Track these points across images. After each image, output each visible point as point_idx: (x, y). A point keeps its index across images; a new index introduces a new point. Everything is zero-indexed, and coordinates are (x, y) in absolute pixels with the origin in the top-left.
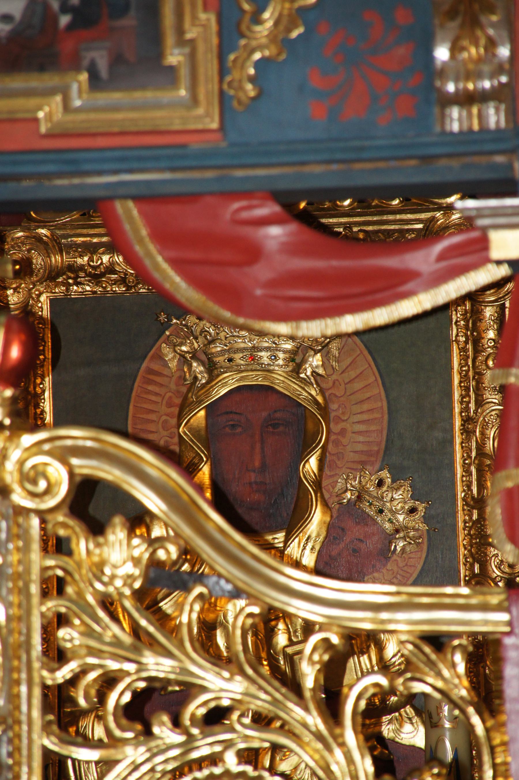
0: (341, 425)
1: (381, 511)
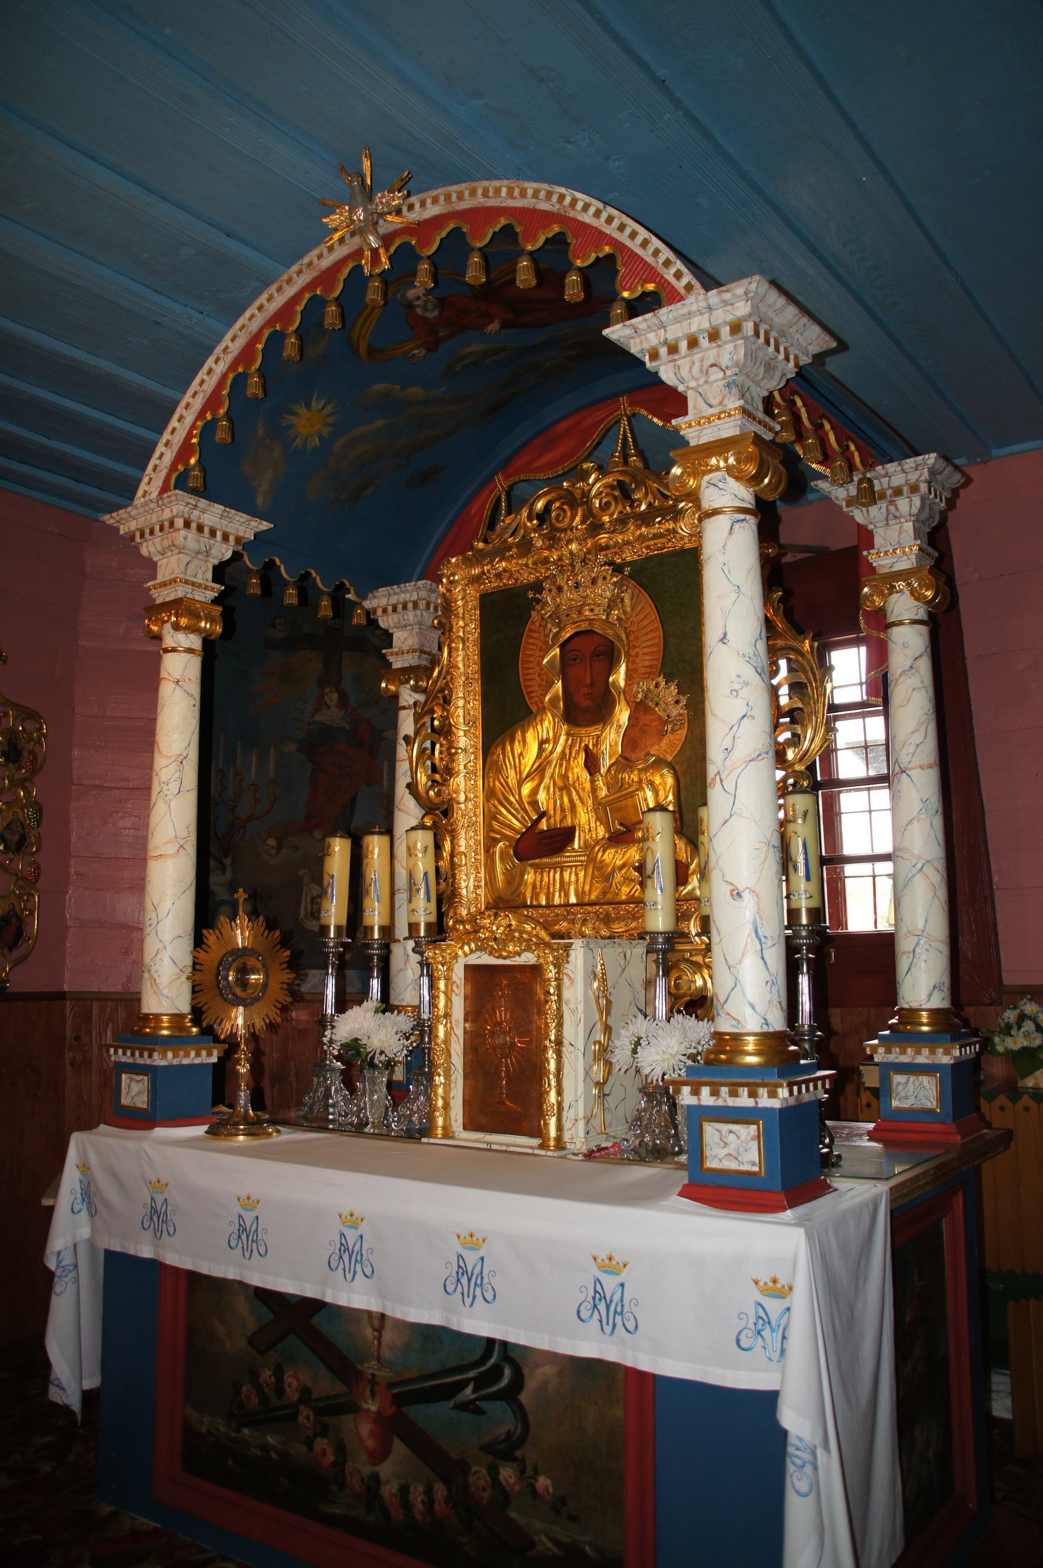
0: (637, 650)
1: (657, 704)
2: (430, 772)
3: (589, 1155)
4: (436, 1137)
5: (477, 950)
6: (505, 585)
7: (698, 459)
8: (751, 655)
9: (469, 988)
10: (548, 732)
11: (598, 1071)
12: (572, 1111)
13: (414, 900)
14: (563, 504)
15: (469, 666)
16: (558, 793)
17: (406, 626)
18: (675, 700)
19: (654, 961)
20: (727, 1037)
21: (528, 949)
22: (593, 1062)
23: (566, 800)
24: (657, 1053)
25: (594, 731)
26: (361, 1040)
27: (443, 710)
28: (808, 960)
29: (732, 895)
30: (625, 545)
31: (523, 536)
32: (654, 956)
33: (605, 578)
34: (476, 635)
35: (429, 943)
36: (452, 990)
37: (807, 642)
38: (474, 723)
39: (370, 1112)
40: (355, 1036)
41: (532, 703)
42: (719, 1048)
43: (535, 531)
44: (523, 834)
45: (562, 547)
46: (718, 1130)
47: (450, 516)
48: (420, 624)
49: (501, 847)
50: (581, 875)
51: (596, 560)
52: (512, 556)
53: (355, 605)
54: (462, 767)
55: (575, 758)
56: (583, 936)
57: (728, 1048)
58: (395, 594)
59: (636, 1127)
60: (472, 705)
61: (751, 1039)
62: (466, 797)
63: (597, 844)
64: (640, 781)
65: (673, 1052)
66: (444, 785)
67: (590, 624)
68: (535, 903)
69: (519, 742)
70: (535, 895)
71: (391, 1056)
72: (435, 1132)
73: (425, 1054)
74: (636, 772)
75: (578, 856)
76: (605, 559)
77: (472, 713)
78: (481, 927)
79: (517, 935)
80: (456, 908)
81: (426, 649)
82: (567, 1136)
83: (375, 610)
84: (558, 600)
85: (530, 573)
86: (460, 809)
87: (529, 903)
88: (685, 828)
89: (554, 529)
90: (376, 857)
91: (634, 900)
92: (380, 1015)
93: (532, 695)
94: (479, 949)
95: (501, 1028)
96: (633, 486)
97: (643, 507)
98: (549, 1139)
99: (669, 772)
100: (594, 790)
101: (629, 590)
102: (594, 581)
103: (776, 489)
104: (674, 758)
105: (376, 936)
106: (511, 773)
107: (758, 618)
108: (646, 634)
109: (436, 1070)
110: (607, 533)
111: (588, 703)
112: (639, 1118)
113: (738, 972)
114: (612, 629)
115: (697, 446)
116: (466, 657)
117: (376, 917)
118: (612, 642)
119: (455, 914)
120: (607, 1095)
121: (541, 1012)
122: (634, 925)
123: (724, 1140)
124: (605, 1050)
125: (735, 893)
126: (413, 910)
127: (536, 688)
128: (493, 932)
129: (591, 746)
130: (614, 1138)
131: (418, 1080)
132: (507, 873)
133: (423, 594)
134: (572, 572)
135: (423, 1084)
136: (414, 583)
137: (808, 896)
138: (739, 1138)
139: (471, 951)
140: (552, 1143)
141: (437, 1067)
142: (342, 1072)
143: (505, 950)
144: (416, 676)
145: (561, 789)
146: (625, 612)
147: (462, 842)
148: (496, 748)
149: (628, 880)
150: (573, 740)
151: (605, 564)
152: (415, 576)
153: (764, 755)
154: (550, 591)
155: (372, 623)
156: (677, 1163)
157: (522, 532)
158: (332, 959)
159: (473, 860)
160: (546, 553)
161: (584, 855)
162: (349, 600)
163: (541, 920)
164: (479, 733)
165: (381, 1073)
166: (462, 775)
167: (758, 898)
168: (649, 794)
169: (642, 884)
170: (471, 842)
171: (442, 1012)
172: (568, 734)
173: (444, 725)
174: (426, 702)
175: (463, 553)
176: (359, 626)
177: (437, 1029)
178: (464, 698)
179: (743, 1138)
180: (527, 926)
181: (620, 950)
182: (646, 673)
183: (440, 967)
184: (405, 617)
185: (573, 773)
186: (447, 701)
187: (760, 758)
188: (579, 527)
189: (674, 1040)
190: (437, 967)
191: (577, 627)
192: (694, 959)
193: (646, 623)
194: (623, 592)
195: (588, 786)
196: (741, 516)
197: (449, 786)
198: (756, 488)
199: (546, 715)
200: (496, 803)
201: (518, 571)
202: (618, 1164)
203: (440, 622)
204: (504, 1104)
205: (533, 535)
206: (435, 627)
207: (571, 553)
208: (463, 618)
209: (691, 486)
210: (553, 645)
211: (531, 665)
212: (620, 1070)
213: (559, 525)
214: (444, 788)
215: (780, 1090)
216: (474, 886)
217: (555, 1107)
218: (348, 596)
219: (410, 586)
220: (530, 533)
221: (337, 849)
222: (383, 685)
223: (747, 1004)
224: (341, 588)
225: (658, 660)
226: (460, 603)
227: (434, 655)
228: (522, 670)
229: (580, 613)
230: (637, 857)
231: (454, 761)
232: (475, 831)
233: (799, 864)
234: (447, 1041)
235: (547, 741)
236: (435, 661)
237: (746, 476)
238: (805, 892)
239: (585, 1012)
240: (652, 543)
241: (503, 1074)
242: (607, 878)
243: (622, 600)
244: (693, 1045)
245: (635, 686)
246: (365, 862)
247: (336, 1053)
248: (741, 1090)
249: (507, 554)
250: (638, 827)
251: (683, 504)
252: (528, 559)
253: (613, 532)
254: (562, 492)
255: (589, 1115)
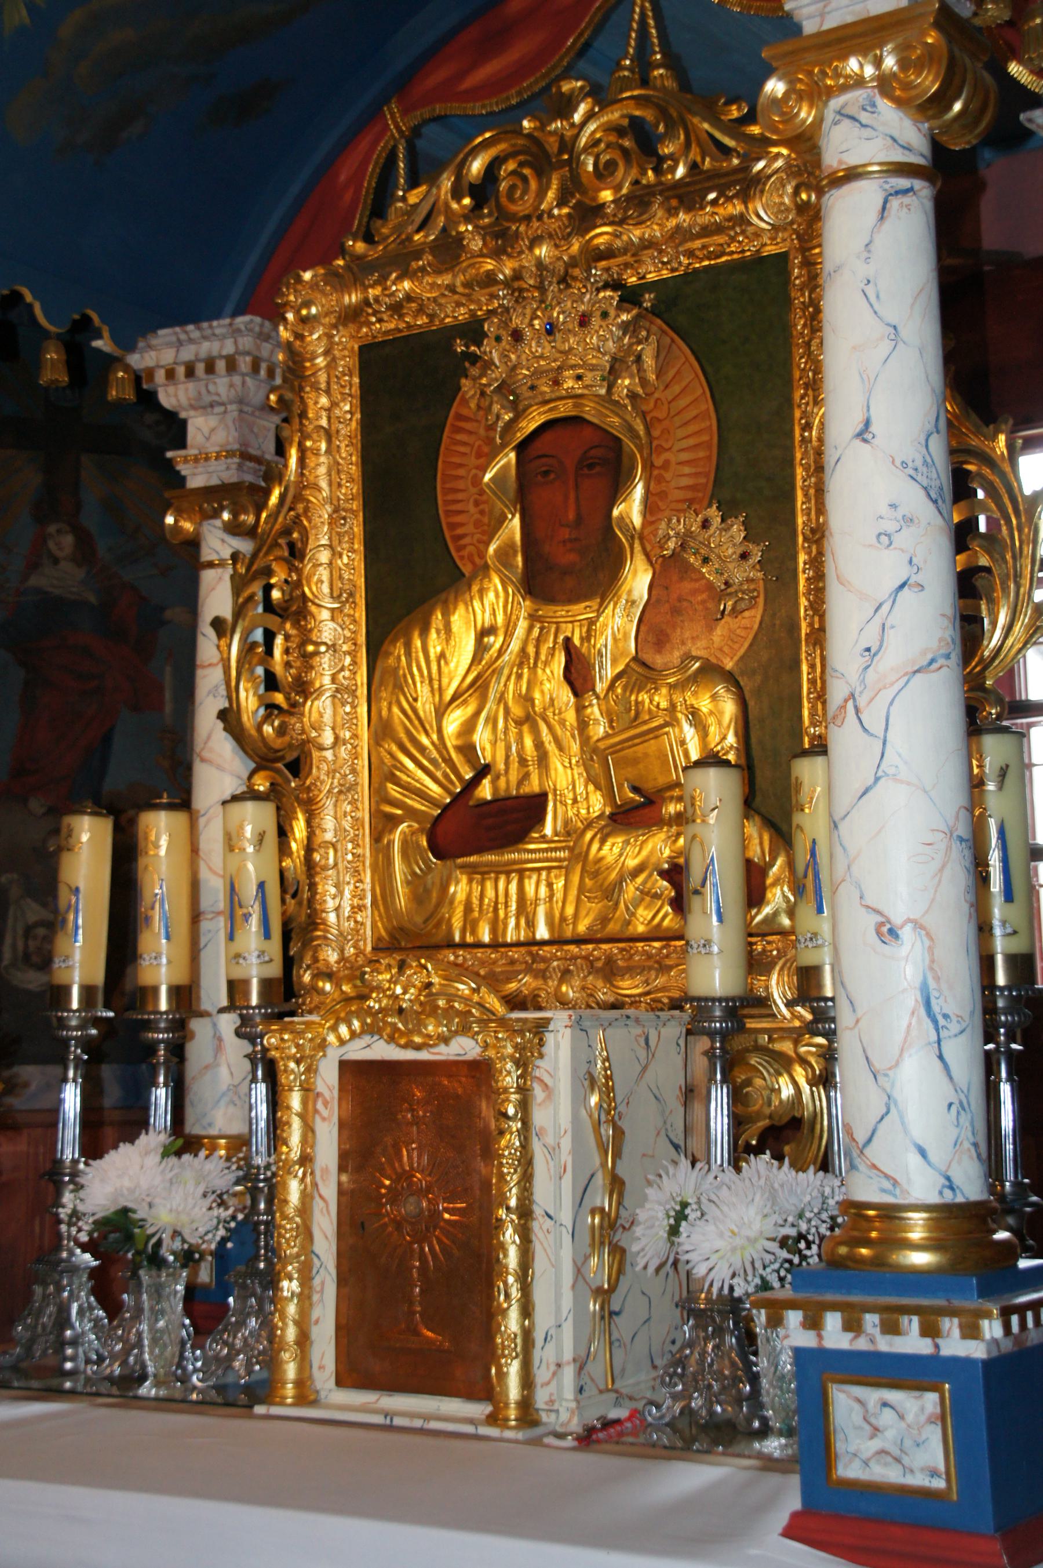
2: (262, 690)
3: (587, 1438)
4: (282, 1404)
5: (363, 1032)
6: (409, 326)
7: (820, 64)
8: (919, 463)
9: (348, 1106)
10: (494, 614)
11: (599, 1268)
12: (551, 1347)
13: (239, 934)
14: (521, 165)
15: (340, 485)
16: (513, 730)
17: (212, 406)
18: (740, 551)
19: (705, 1053)
20: (871, 1213)
21: (465, 1030)
22: (588, 1250)
23: (528, 742)
24: (721, 1235)
25: (582, 611)
26: (134, 1211)
27: (290, 570)
28: (1010, 1054)
29: (879, 933)
30: (646, 248)
31: (444, 230)
32: (704, 1043)
33: (605, 315)
34: (354, 424)
35: (270, 1018)
36: (316, 1111)
37: (1002, 438)
38: (351, 595)
39: (151, 1353)
40: (123, 1203)
41: (462, 558)
42: (856, 1233)
43: (467, 219)
44: (446, 808)
45: (522, 252)
46: (859, 1401)
47: (295, 189)
48: (241, 401)
49: (403, 832)
50: (559, 884)
51: (588, 279)
52: (423, 269)
53: (109, 362)
54: (327, 680)
55: (546, 663)
56: (564, 1003)
57: (874, 1234)
58: (191, 341)
59: (676, 1379)
60: (345, 560)
61: (917, 1218)
62: (337, 738)
63: (589, 826)
64: (673, 707)
65: (752, 1234)
66: (291, 714)
67: (575, 406)
68: (469, 939)
69: (438, 632)
70: (470, 924)
71: (194, 1240)
72: (281, 1392)
73: (259, 1234)
74: (664, 691)
75: (551, 850)
76: (605, 277)
77: (346, 576)
78: (373, 989)
79: (441, 1003)
80: (316, 949)
81: (252, 451)
82: (541, 1398)
83: (150, 373)
84: (513, 357)
85: (459, 304)
86: (325, 759)
87: (457, 938)
88: (758, 799)
89: (503, 215)
90: (163, 852)
91: (660, 935)
92: (173, 1160)
93: (463, 542)
94: (369, 1030)
95: (411, 1184)
96: (661, 128)
97: (680, 171)
98: (507, 1405)
99: (728, 690)
100: (583, 724)
101: (653, 338)
102: (584, 321)
103: (977, 122)
104: (737, 664)
105: (163, 1006)
106: (423, 691)
107: (933, 391)
108: (686, 424)
109: (284, 1267)
110: (610, 224)
111: (572, 557)
112: (681, 1362)
113: (893, 1085)
114: (618, 415)
115: (819, 34)
116: (335, 468)
117: (164, 970)
118: (618, 440)
119: (316, 960)
120: (617, 1314)
121: (489, 1152)
122: (660, 982)
123: (873, 1420)
124: (612, 1226)
125: (885, 929)
126: (238, 956)
127: (469, 528)
128: (397, 997)
129: (577, 641)
130: (631, 1398)
131: (244, 1286)
132: (414, 881)
133: (246, 342)
134: (542, 301)
135: (254, 1294)
136: (227, 321)
137: (1009, 930)
138: (902, 1417)
139: (353, 1035)
140: (512, 1414)
141: (286, 1261)
142: (93, 1273)
143: (419, 1033)
144: (234, 503)
145: (519, 723)
146: (644, 382)
147: (329, 823)
148: (394, 642)
149: (648, 895)
150: (542, 629)
151: (606, 286)
152: (230, 307)
153: (941, 661)
154: (498, 339)
155: (147, 398)
156: (760, 1456)
157: (441, 221)
158: (75, 1051)
159: (350, 857)
160: (489, 265)
161: (563, 849)
162: (98, 351)
163: (482, 972)
164: (361, 614)
165: (173, 1275)
166: (328, 694)
167: (931, 939)
168: (689, 732)
169: (679, 904)
170: (347, 823)
171: (295, 1155)
172: (533, 618)
173: (291, 599)
174: (255, 555)
175: (325, 260)
176: (120, 403)
177: (285, 1185)
178: (331, 546)
179: (910, 1418)
180: (461, 986)
181: (638, 1031)
182: (684, 501)
183: (292, 1065)
184: (211, 388)
185: (542, 692)
186: (296, 553)
187: (935, 666)
188: (556, 212)
189: (752, 1211)
190: (286, 1066)
191: (551, 410)
192: (778, 1046)
193: (682, 403)
194: (639, 343)
195: (571, 716)
196: (904, 183)
197: (303, 715)
198: (936, 123)
199: (490, 581)
200: (394, 748)
201: (435, 300)
202: (655, 1457)
203: (281, 400)
204: (417, 1333)
205: (462, 228)
206: (272, 409)
207: (540, 264)
208: (328, 392)
209: (804, 121)
210: (504, 446)
211: (461, 484)
212: (645, 1267)
213: (513, 208)
214: (293, 720)
215: (985, 1324)
216: (353, 907)
217: (519, 1341)
218: (97, 344)
219: (219, 326)
220: (458, 223)
221: (85, 837)
222: (170, 520)
223: (913, 1149)
224: (83, 327)
225: (707, 475)
226: (320, 361)
227: (268, 463)
228: (444, 494)
229: (556, 383)
230: (667, 853)
231: (312, 668)
232: (353, 802)
233: (991, 869)
234: (305, 1210)
235: (491, 630)
236: (273, 475)
237: (917, 96)
238: (1004, 923)
239: (575, 1152)
240: (698, 244)
241: (415, 1275)
242: (611, 892)
243: (639, 359)
244: (790, 1219)
245: (663, 525)
246: (142, 861)
247: (84, 1237)
248: (904, 1320)
249: (414, 265)
250: (668, 794)
251: (761, 165)
252: (455, 276)
253: (621, 222)
254: (521, 142)
255: (583, 1354)
